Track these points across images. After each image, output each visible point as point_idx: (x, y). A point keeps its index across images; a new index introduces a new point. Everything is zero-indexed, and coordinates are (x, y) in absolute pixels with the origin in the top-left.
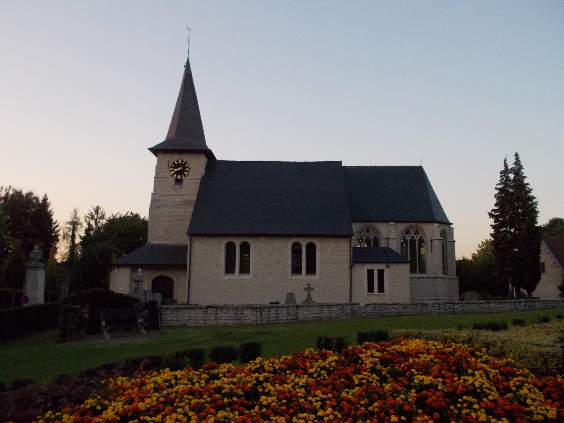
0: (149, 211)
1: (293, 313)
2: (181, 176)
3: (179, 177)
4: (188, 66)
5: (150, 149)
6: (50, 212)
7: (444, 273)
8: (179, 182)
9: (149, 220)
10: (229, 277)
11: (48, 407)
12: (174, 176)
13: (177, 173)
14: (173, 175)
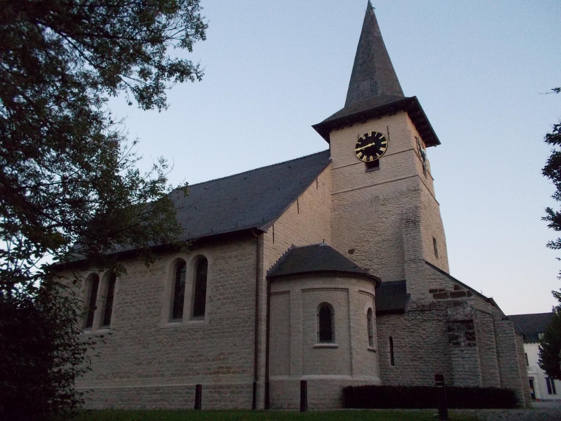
0: (446, 251)
1: (93, 195)
2: (374, 155)
3: (371, 158)
4: (370, 8)
5: (315, 127)
6: (548, 162)
7: (550, 392)
8: (373, 166)
9: (522, 349)
10: (175, 324)
11: (48, 402)
12: (363, 160)
13: (365, 152)
14: (362, 157)
